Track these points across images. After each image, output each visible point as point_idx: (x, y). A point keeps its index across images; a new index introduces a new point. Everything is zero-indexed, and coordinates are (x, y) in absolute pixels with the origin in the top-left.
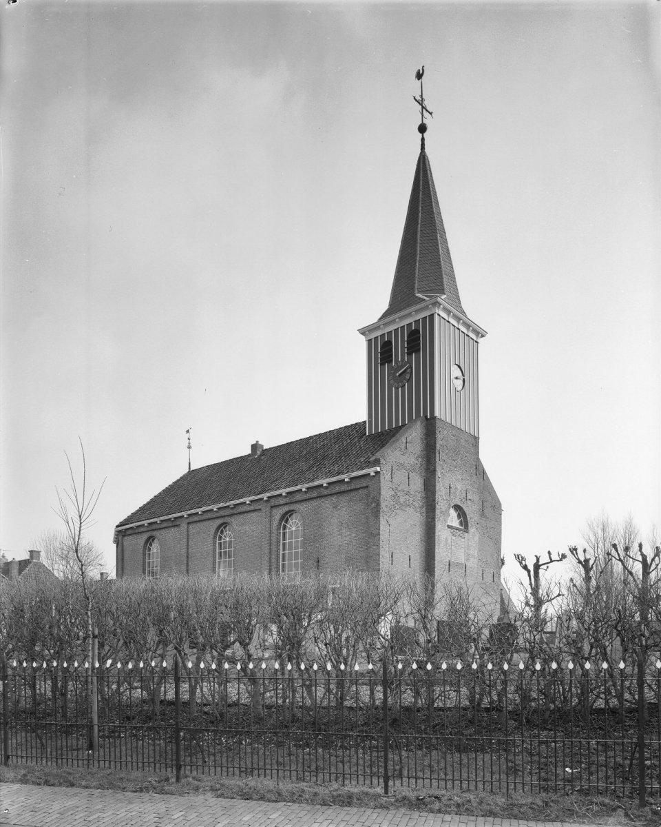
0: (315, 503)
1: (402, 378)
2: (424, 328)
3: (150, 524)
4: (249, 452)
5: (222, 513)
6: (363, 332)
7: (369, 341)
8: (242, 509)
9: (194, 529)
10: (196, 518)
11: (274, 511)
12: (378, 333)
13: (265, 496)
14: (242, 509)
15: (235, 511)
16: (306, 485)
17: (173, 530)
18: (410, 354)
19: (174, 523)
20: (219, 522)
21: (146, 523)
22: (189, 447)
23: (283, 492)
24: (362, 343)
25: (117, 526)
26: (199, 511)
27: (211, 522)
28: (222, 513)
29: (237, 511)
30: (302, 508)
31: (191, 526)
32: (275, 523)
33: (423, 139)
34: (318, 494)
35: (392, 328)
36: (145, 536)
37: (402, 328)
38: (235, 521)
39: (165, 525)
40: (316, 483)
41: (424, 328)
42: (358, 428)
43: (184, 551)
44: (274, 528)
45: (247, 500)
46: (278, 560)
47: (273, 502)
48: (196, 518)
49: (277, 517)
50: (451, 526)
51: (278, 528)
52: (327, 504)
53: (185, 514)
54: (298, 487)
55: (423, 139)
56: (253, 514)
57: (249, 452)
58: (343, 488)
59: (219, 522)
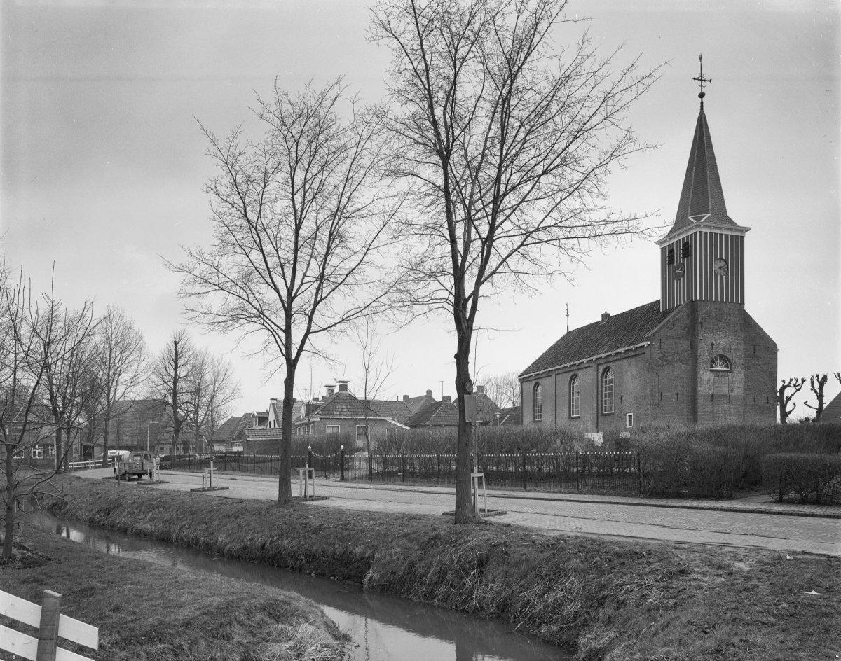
0: (620, 362)
1: (678, 277)
2: (677, 246)
3: (536, 375)
4: (600, 319)
5: (573, 368)
6: (657, 243)
7: (662, 249)
8: (582, 366)
9: (559, 378)
10: (559, 371)
11: (600, 367)
12: (667, 244)
13: (594, 358)
14: (582, 366)
15: (579, 367)
16: (587, 359)
17: (548, 378)
18: (683, 258)
19: (548, 374)
20: (572, 373)
21: (533, 374)
22: (567, 316)
23: (603, 355)
24: (658, 249)
25: (522, 375)
26: (561, 367)
27: (567, 374)
28: (573, 368)
29: (580, 367)
30: (612, 365)
31: (558, 376)
32: (600, 375)
33: (702, 103)
34: (620, 357)
35: (674, 241)
36: (534, 382)
37: (680, 240)
38: (579, 373)
39: (544, 375)
40: (619, 350)
41: (677, 246)
42: (652, 308)
43: (554, 392)
44: (600, 378)
45: (585, 360)
46: (602, 398)
47: (599, 362)
48: (559, 371)
49: (601, 371)
50: (463, 403)
51: (602, 378)
52: (625, 362)
53: (553, 369)
54: (610, 353)
55: (702, 103)
56: (589, 369)
57: (600, 319)
58: (633, 353)
59: (572, 373)
